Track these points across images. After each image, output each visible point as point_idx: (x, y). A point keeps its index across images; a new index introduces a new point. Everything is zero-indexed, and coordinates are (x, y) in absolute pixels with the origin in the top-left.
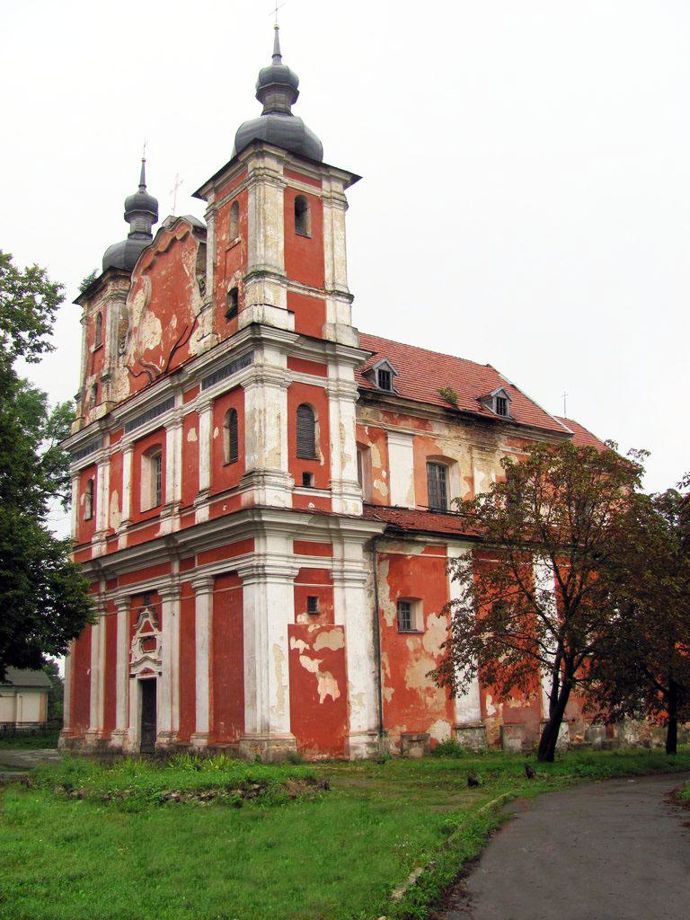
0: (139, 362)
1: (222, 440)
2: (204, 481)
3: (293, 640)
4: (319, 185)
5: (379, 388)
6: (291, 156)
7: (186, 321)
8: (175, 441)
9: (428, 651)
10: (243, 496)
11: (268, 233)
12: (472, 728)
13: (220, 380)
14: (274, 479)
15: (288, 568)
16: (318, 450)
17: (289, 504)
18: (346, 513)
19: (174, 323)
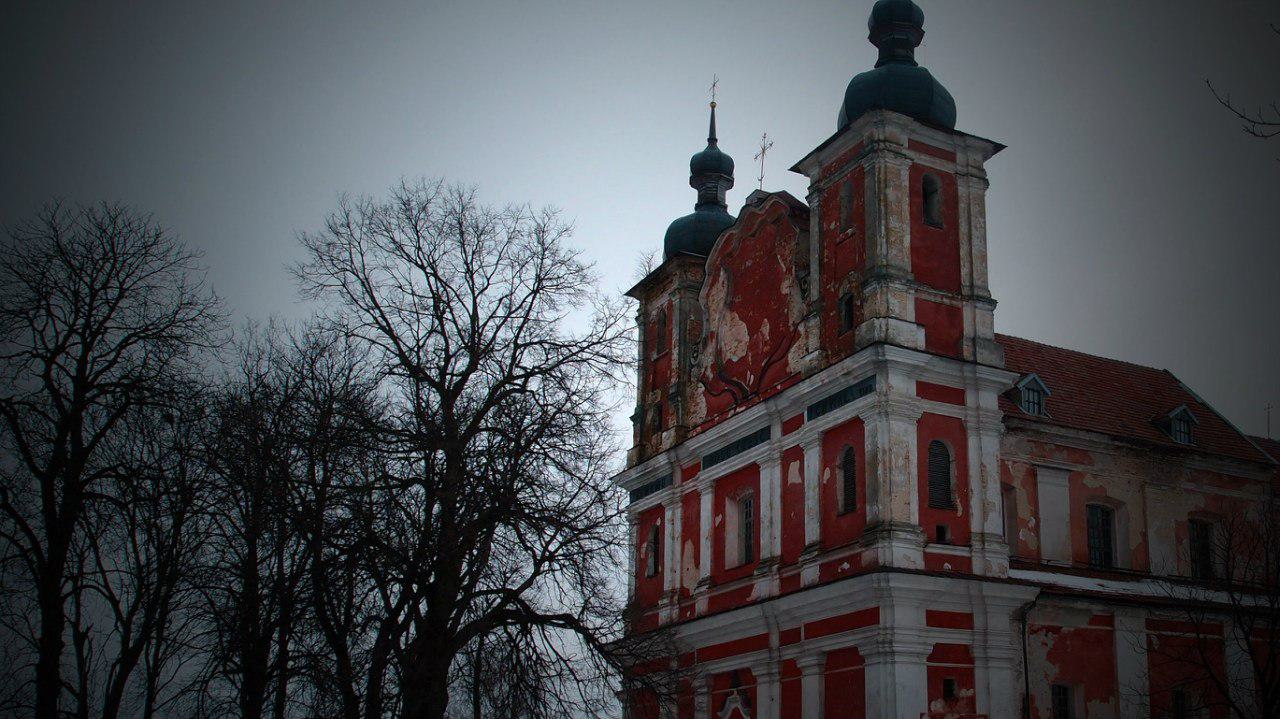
2: (812, 532)
4: (950, 157)
8: (772, 483)
14: (902, 535)
17: (920, 564)
18: (989, 574)
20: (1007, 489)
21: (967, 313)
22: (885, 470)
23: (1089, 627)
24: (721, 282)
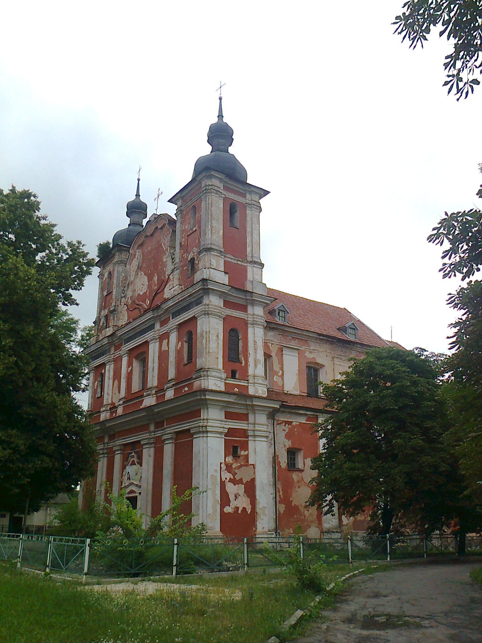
2: (172, 373)
14: (214, 374)
17: (223, 389)
18: (257, 395)
20: (267, 356)
21: (249, 269)
22: (206, 341)
23: (306, 422)
24: (136, 258)
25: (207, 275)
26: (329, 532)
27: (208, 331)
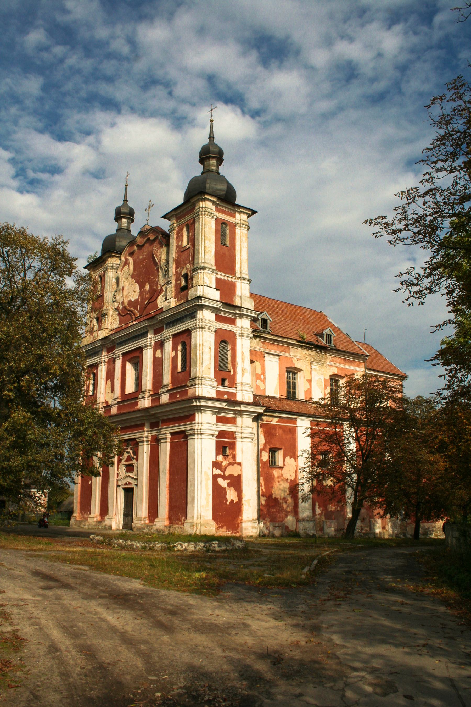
0: (125, 307)
1: (177, 358)
2: (167, 379)
3: (214, 469)
5: (261, 329)
6: (220, 201)
7: (155, 287)
9: (285, 477)
10: (189, 390)
11: (206, 245)
12: (307, 521)
13: (176, 325)
14: (207, 382)
15: (213, 430)
16: (230, 366)
17: (214, 396)
18: (244, 401)
19: (147, 287)
25: (200, 292)
26: (303, 520)
27: (201, 343)
